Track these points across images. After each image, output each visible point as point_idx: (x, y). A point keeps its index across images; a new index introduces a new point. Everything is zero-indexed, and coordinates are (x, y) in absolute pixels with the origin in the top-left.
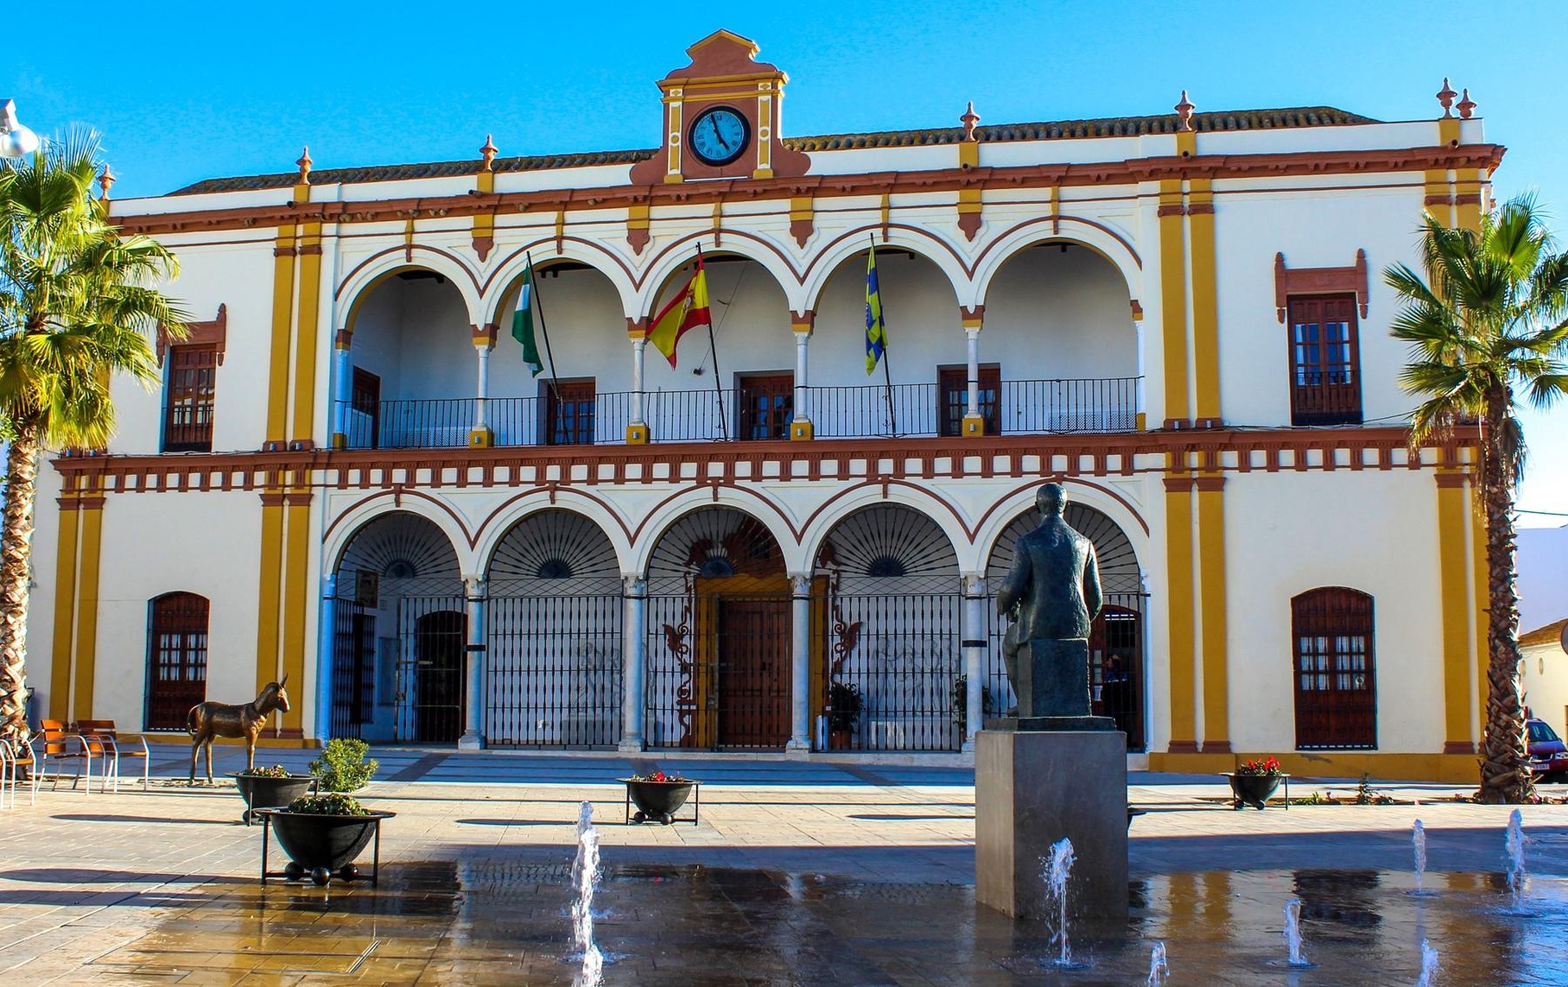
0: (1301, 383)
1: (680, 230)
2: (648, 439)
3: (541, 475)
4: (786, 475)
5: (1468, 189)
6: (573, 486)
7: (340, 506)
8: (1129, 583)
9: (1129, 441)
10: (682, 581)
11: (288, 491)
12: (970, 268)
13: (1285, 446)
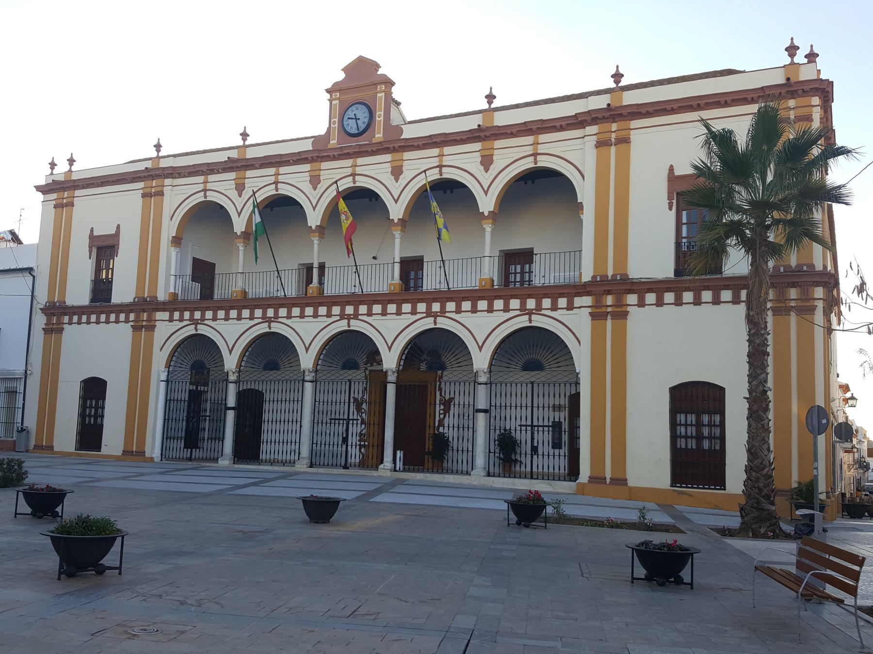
0: (685, 249)
1: (338, 175)
2: (493, 286)
4: (384, 313)
5: (802, 112)
7: (168, 332)
9: (572, 291)
11: (144, 323)
13: (669, 290)
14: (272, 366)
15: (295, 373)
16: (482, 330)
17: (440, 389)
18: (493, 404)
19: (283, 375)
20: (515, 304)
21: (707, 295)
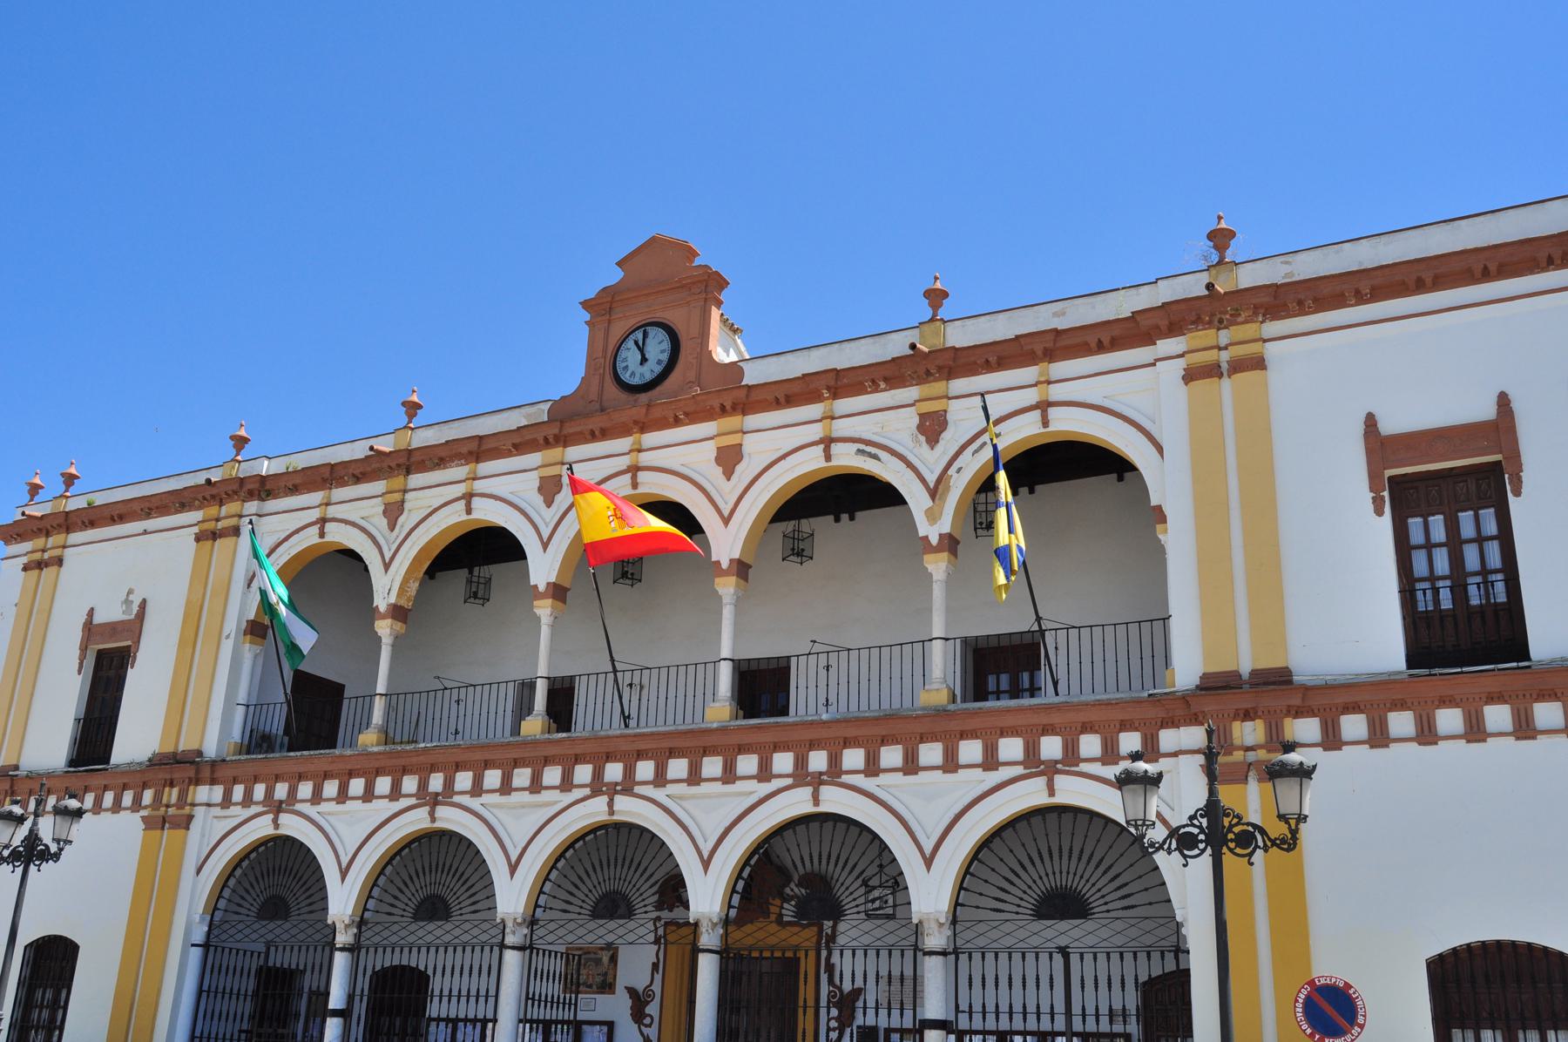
3: (801, 762)
6: (1084, 767)
7: (224, 829)
8: (1162, 932)
10: (650, 926)
11: (171, 811)
12: (726, 513)
14: (434, 909)
15: (485, 926)
16: (934, 814)
17: (830, 968)
18: (964, 1006)
19: (457, 932)
20: (1011, 748)
21: (1498, 716)
